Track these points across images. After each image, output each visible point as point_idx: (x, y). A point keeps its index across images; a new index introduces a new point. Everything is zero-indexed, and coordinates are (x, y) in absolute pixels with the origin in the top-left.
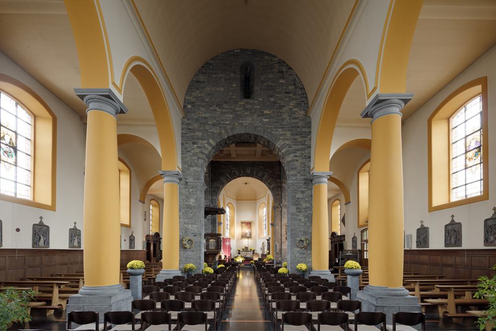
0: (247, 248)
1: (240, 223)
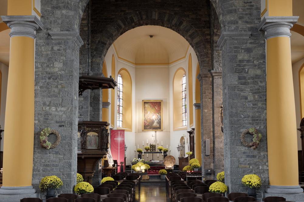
0: (153, 147)
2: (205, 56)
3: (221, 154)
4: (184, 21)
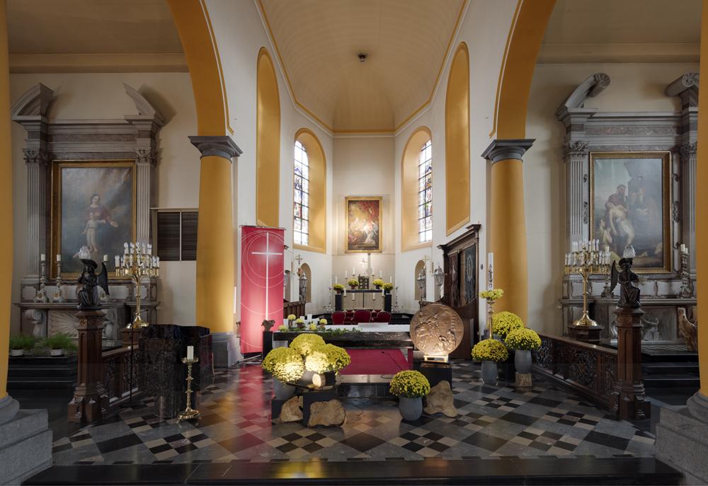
0: (364, 281)
1: (343, 204)
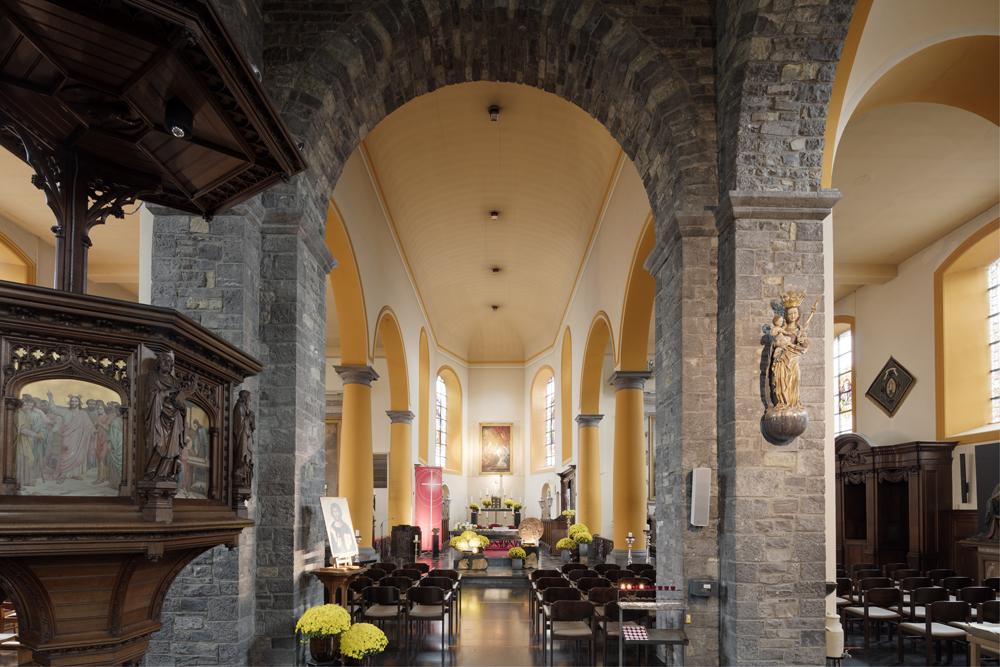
0: (496, 500)
1: (478, 428)
2: (693, 153)
3: (758, 523)
4: (617, 17)
